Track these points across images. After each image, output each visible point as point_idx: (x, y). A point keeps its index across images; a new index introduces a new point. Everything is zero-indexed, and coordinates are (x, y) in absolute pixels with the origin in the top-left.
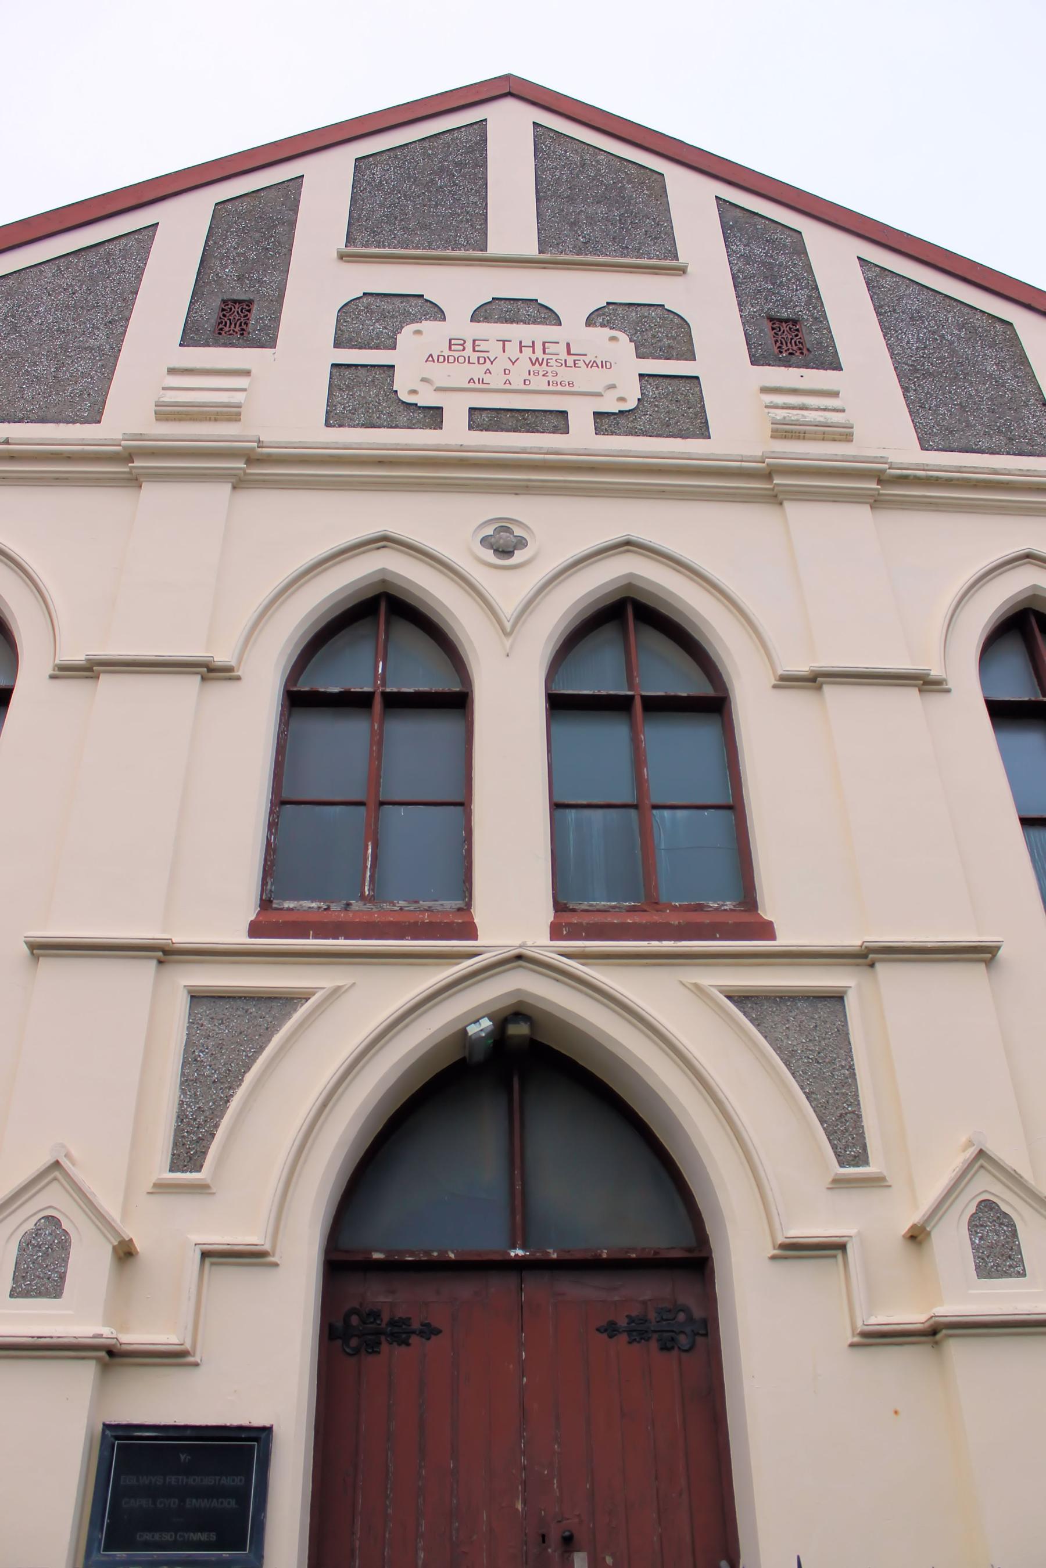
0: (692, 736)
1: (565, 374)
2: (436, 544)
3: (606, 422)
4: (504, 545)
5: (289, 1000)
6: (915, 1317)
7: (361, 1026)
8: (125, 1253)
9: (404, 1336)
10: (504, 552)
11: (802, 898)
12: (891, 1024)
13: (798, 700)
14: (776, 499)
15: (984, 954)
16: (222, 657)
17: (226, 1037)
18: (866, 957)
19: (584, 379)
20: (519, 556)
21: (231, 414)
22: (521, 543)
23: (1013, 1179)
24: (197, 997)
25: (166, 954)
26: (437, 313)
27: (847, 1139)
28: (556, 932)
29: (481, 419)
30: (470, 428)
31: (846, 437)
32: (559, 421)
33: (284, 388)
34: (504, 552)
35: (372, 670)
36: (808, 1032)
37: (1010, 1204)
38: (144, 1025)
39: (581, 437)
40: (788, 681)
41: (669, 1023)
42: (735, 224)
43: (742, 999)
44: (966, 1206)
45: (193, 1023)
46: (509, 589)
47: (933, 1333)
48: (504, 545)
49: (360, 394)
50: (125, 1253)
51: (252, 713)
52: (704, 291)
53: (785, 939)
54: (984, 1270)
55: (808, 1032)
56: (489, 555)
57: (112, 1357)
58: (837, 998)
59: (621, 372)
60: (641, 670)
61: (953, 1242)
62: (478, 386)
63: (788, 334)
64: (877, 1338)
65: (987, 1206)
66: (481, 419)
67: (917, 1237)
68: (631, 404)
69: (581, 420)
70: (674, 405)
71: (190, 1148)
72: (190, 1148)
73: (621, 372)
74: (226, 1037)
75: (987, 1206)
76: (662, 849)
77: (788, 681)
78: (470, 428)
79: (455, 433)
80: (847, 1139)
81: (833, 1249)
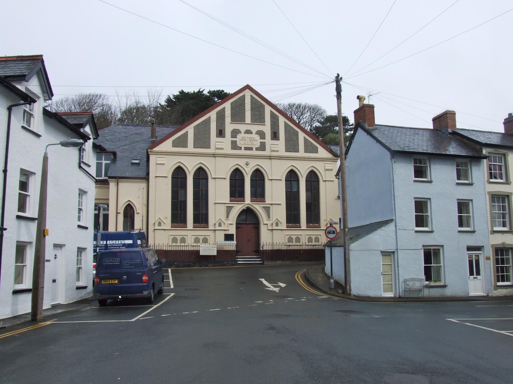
0: (204, 181)
2: (241, 163)
3: (257, 149)
5: (233, 207)
7: (238, 208)
9: (347, 230)
10: (247, 165)
11: (268, 199)
12: (274, 210)
13: (214, 180)
14: (271, 159)
17: (229, 209)
18: (272, 204)
25: (224, 203)
27: (269, 217)
28: (251, 201)
29: (246, 149)
32: (251, 149)
34: (247, 165)
35: (237, 177)
36: (267, 210)
37: (222, 222)
38: (222, 209)
39: (254, 152)
40: (212, 178)
41: (258, 208)
44: (158, 222)
45: (393, 210)
49: (234, 146)
51: (283, 183)
53: (266, 203)
54: (159, 226)
55: (267, 210)
59: (257, 141)
60: (258, 177)
61: (274, 224)
63: (275, 136)
70: (262, 147)
71: (227, 217)
72: (227, 217)
73: (257, 141)
74: (229, 209)
76: (259, 193)
77: (212, 178)
79: (243, 152)
80: (269, 217)
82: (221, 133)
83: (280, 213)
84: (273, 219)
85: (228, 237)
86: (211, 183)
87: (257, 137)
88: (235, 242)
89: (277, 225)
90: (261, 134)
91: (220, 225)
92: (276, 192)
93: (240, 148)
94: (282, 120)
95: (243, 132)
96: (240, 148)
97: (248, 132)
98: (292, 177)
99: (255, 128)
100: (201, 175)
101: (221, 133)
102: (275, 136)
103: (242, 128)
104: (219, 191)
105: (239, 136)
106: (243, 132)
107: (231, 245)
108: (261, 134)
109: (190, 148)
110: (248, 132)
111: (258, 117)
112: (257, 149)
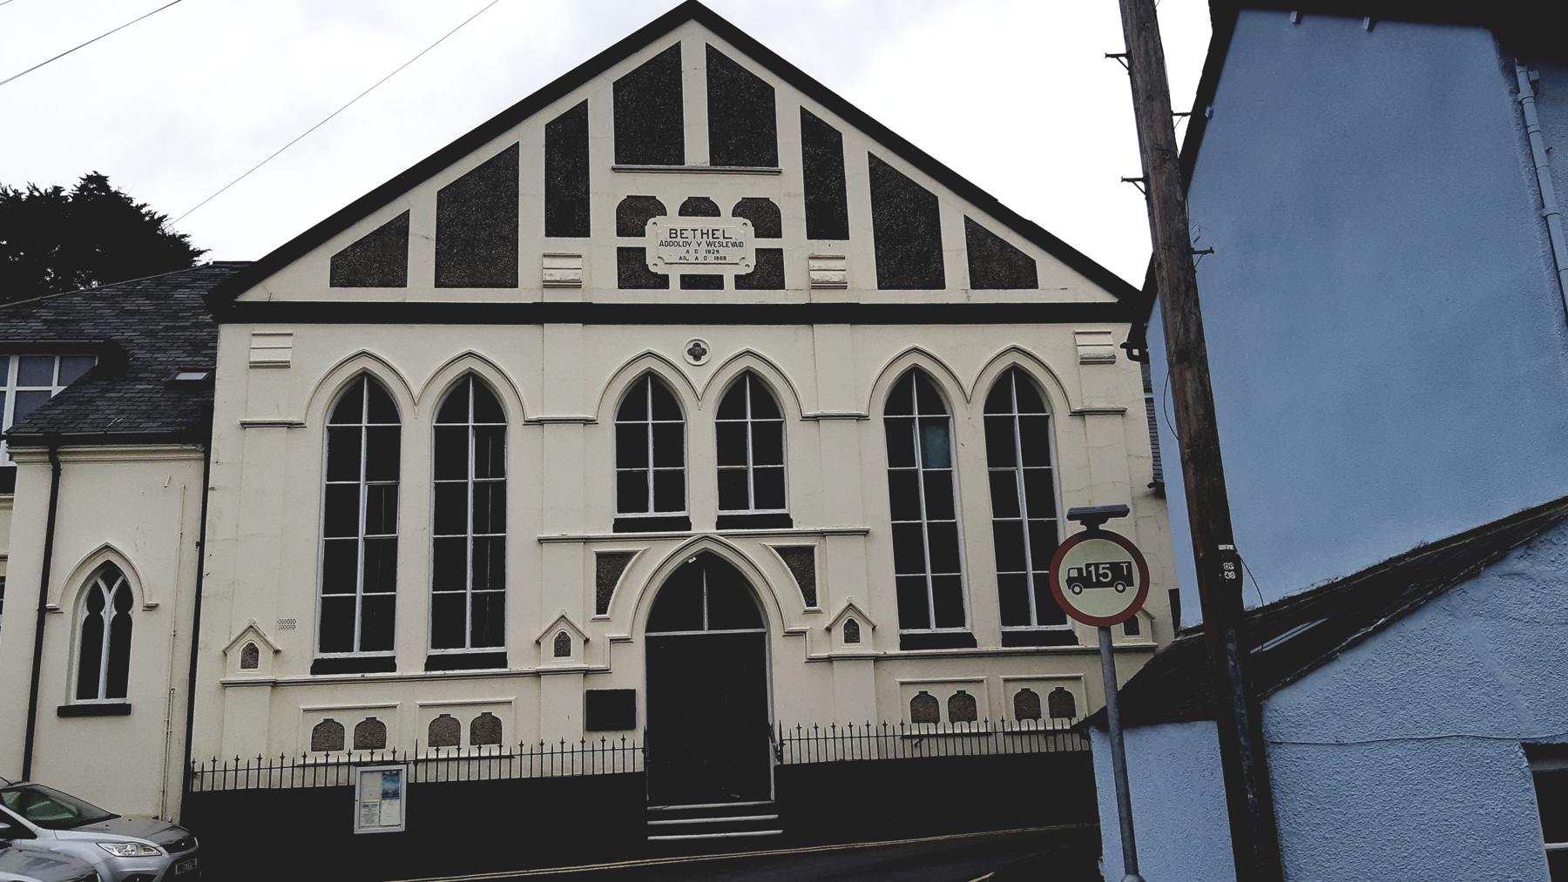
1: (723, 252)
3: (742, 282)
4: (697, 352)
5: (629, 555)
6: (825, 654)
7: (653, 560)
8: (587, 641)
12: (830, 562)
13: (811, 425)
15: (865, 533)
16: (590, 417)
17: (610, 568)
19: (731, 254)
20: (704, 359)
21: (575, 285)
22: (704, 352)
23: (859, 613)
24: (600, 556)
25: (587, 540)
26: (662, 210)
27: (810, 598)
29: (689, 282)
30: (332, 285)
31: (841, 286)
32: (715, 282)
33: (591, 267)
34: (697, 358)
36: (801, 562)
39: (730, 295)
41: (758, 557)
42: (812, 129)
43: (780, 550)
46: (700, 375)
47: (830, 659)
48: (697, 352)
49: (633, 268)
50: (587, 641)
52: (786, 187)
55: (801, 562)
56: (690, 359)
57: (587, 673)
58: (810, 549)
59: (744, 246)
60: (752, 410)
61: (839, 632)
62: (683, 261)
63: (827, 220)
64: (811, 660)
65: (851, 621)
66: (689, 282)
67: (828, 630)
68: (750, 270)
69: (729, 282)
70: (769, 270)
71: (602, 607)
72: (602, 607)
73: (744, 246)
74: (610, 568)
75: (851, 621)
78: (332, 285)
79: (673, 295)
80: (810, 598)
81: (803, 633)
82: (568, 216)
83: (863, 578)
84: (832, 602)
85: (606, 710)
86: (519, 445)
87: (742, 229)
88: (637, 737)
89: (852, 634)
90: (763, 216)
91: (562, 647)
92: (837, 480)
93: (662, 282)
94: (856, 151)
95: (673, 207)
96: (662, 282)
97: (698, 207)
98: (914, 403)
99: (729, 189)
100: (473, 410)
101: (568, 216)
102: (827, 220)
103: (669, 188)
104: (560, 486)
105: (657, 229)
106: (673, 207)
107: (624, 752)
108: (763, 216)
109: (420, 285)
110: (698, 207)
111: (743, 135)
112: (742, 282)
